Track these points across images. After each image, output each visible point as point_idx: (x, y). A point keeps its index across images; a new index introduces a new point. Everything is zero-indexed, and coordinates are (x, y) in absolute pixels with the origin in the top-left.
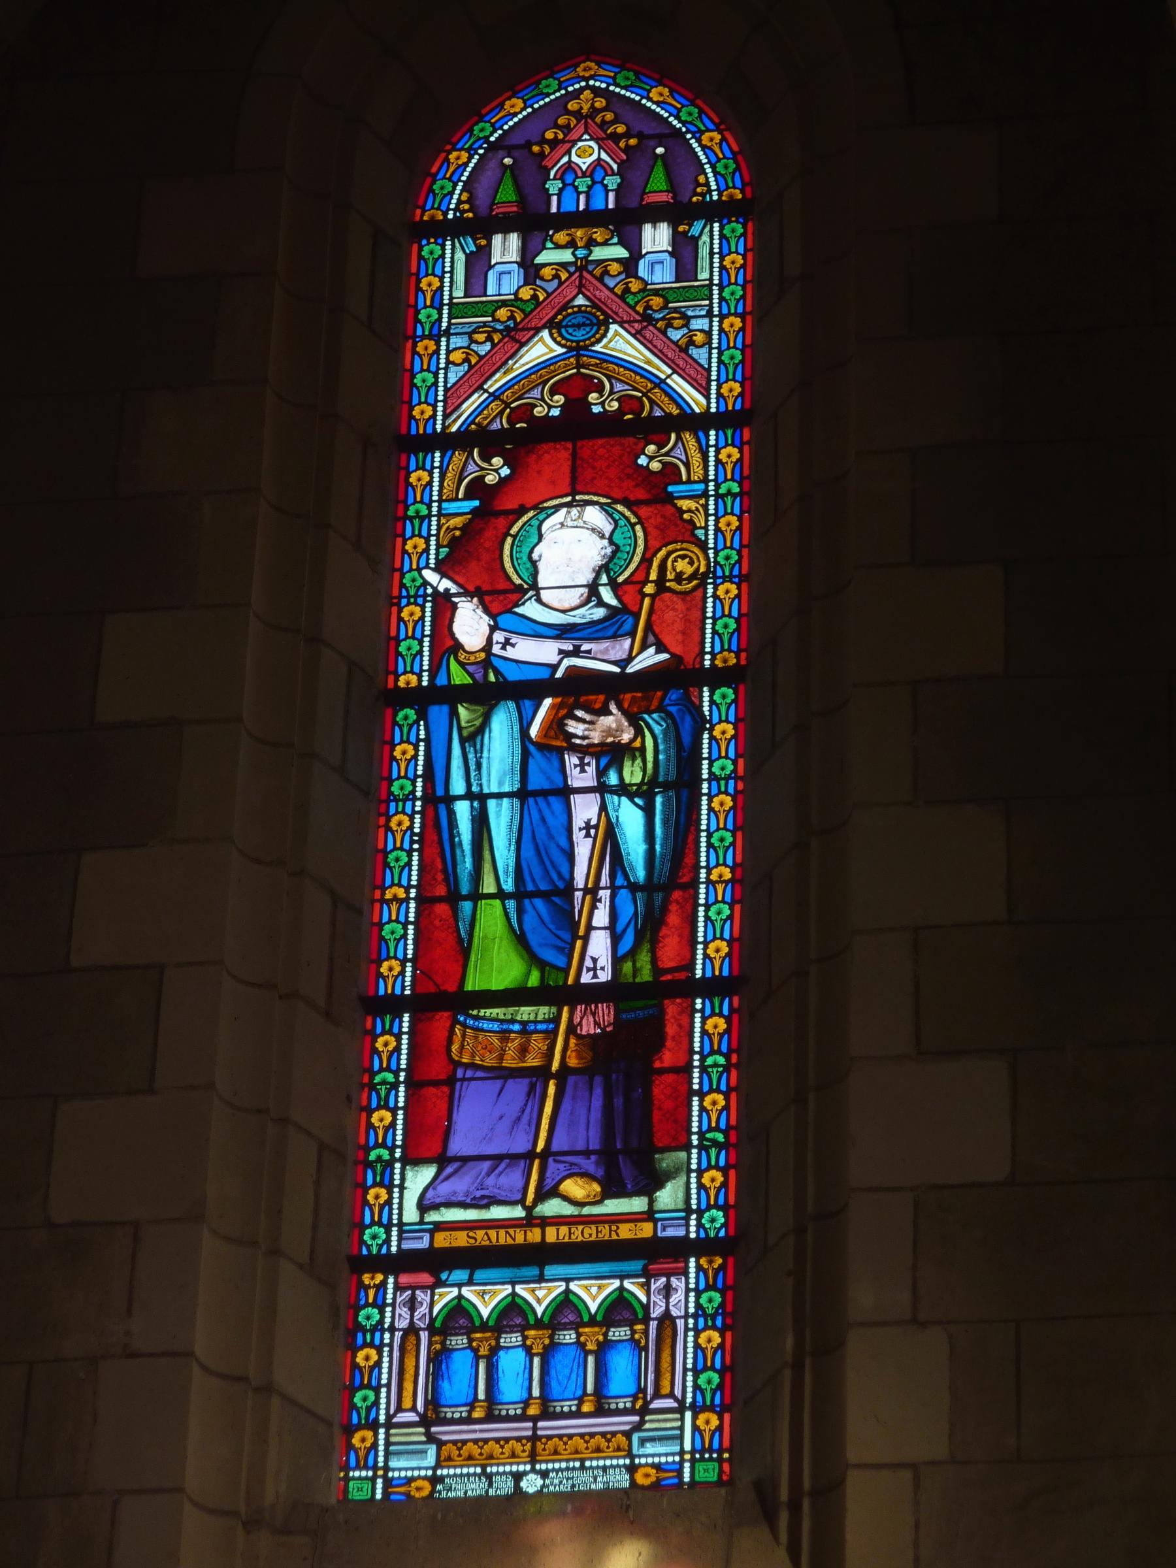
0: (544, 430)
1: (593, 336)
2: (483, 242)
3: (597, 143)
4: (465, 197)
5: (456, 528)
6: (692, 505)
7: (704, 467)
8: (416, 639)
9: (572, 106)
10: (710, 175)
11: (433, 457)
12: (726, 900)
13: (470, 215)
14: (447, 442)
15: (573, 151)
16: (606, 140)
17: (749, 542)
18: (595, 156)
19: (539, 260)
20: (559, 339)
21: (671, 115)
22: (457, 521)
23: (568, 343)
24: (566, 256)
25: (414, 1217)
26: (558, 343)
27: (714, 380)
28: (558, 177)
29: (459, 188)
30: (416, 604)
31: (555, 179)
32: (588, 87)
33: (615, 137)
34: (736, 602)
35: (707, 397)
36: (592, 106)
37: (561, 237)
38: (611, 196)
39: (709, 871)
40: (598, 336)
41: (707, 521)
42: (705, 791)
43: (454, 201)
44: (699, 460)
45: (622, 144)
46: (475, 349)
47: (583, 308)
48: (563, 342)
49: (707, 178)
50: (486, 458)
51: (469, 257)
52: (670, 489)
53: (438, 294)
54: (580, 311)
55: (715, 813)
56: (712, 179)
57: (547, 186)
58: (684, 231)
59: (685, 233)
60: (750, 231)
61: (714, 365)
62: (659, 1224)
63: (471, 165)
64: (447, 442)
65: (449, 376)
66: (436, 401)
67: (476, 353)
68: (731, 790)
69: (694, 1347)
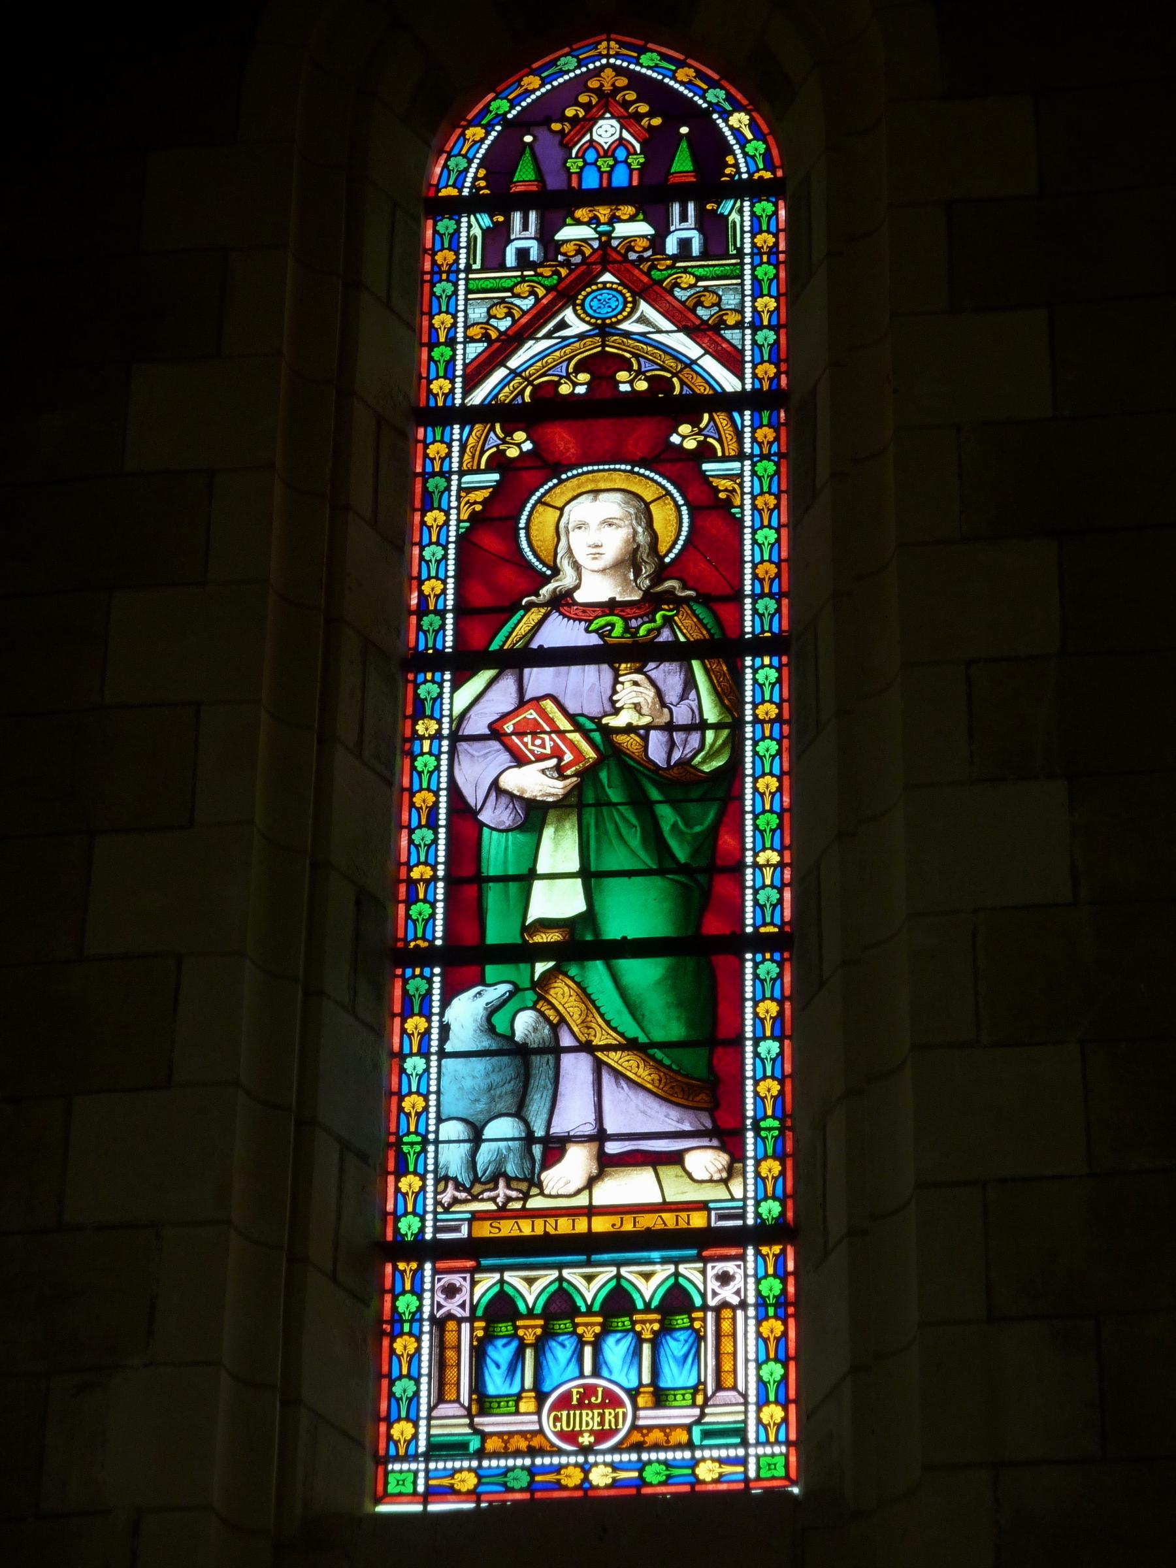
0: (572, 407)
1: (620, 313)
2: (501, 219)
3: (619, 121)
4: (482, 173)
5: (475, 503)
6: (728, 484)
7: (737, 438)
8: (450, 314)
9: (593, 84)
10: (740, 156)
11: (436, 888)
12: (772, 294)
13: (487, 191)
14: (469, 416)
15: (594, 130)
16: (628, 120)
17: (789, 588)
18: (617, 136)
19: (559, 236)
20: (583, 316)
21: (695, 94)
22: (480, 496)
23: (593, 321)
24: (586, 232)
25: (446, 1151)
26: (583, 320)
27: (747, 232)
28: (580, 155)
29: (474, 165)
30: (448, 280)
31: (577, 157)
32: (608, 65)
33: (638, 117)
34: (777, 760)
35: (741, 378)
36: (613, 85)
37: (581, 213)
38: (635, 175)
39: (756, 855)
40: (625, 314)
41: (742, 500)
42: (749, 735)
43: (469, 179)
44: (732, 433)
45: (645, 122)
46: (495, 324)
47: (608, 285)
48: (587, 319)
49: (736, 159)
50: (509, 432)
51: (486, 232)
52: (705, 466)
53: (426, 1001)
54: (605, 288)
55: (760, 546)
56: (741, 161)
57: (568, 165)
58: (713, 209)
59: (714, 211)
60: (783, 470)
61: (748, 347)
62: (713, 1213)
63: (488, 142)
64: (469, 416)
65: (467, 351)
66: (420, 1375)
67: (496, 328)
68: (776, 734)
69: (751, 345)
